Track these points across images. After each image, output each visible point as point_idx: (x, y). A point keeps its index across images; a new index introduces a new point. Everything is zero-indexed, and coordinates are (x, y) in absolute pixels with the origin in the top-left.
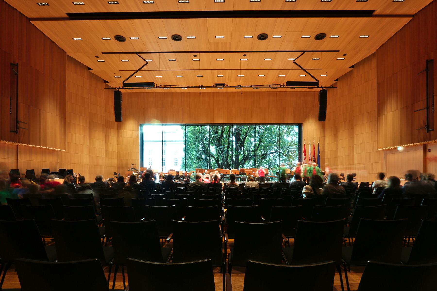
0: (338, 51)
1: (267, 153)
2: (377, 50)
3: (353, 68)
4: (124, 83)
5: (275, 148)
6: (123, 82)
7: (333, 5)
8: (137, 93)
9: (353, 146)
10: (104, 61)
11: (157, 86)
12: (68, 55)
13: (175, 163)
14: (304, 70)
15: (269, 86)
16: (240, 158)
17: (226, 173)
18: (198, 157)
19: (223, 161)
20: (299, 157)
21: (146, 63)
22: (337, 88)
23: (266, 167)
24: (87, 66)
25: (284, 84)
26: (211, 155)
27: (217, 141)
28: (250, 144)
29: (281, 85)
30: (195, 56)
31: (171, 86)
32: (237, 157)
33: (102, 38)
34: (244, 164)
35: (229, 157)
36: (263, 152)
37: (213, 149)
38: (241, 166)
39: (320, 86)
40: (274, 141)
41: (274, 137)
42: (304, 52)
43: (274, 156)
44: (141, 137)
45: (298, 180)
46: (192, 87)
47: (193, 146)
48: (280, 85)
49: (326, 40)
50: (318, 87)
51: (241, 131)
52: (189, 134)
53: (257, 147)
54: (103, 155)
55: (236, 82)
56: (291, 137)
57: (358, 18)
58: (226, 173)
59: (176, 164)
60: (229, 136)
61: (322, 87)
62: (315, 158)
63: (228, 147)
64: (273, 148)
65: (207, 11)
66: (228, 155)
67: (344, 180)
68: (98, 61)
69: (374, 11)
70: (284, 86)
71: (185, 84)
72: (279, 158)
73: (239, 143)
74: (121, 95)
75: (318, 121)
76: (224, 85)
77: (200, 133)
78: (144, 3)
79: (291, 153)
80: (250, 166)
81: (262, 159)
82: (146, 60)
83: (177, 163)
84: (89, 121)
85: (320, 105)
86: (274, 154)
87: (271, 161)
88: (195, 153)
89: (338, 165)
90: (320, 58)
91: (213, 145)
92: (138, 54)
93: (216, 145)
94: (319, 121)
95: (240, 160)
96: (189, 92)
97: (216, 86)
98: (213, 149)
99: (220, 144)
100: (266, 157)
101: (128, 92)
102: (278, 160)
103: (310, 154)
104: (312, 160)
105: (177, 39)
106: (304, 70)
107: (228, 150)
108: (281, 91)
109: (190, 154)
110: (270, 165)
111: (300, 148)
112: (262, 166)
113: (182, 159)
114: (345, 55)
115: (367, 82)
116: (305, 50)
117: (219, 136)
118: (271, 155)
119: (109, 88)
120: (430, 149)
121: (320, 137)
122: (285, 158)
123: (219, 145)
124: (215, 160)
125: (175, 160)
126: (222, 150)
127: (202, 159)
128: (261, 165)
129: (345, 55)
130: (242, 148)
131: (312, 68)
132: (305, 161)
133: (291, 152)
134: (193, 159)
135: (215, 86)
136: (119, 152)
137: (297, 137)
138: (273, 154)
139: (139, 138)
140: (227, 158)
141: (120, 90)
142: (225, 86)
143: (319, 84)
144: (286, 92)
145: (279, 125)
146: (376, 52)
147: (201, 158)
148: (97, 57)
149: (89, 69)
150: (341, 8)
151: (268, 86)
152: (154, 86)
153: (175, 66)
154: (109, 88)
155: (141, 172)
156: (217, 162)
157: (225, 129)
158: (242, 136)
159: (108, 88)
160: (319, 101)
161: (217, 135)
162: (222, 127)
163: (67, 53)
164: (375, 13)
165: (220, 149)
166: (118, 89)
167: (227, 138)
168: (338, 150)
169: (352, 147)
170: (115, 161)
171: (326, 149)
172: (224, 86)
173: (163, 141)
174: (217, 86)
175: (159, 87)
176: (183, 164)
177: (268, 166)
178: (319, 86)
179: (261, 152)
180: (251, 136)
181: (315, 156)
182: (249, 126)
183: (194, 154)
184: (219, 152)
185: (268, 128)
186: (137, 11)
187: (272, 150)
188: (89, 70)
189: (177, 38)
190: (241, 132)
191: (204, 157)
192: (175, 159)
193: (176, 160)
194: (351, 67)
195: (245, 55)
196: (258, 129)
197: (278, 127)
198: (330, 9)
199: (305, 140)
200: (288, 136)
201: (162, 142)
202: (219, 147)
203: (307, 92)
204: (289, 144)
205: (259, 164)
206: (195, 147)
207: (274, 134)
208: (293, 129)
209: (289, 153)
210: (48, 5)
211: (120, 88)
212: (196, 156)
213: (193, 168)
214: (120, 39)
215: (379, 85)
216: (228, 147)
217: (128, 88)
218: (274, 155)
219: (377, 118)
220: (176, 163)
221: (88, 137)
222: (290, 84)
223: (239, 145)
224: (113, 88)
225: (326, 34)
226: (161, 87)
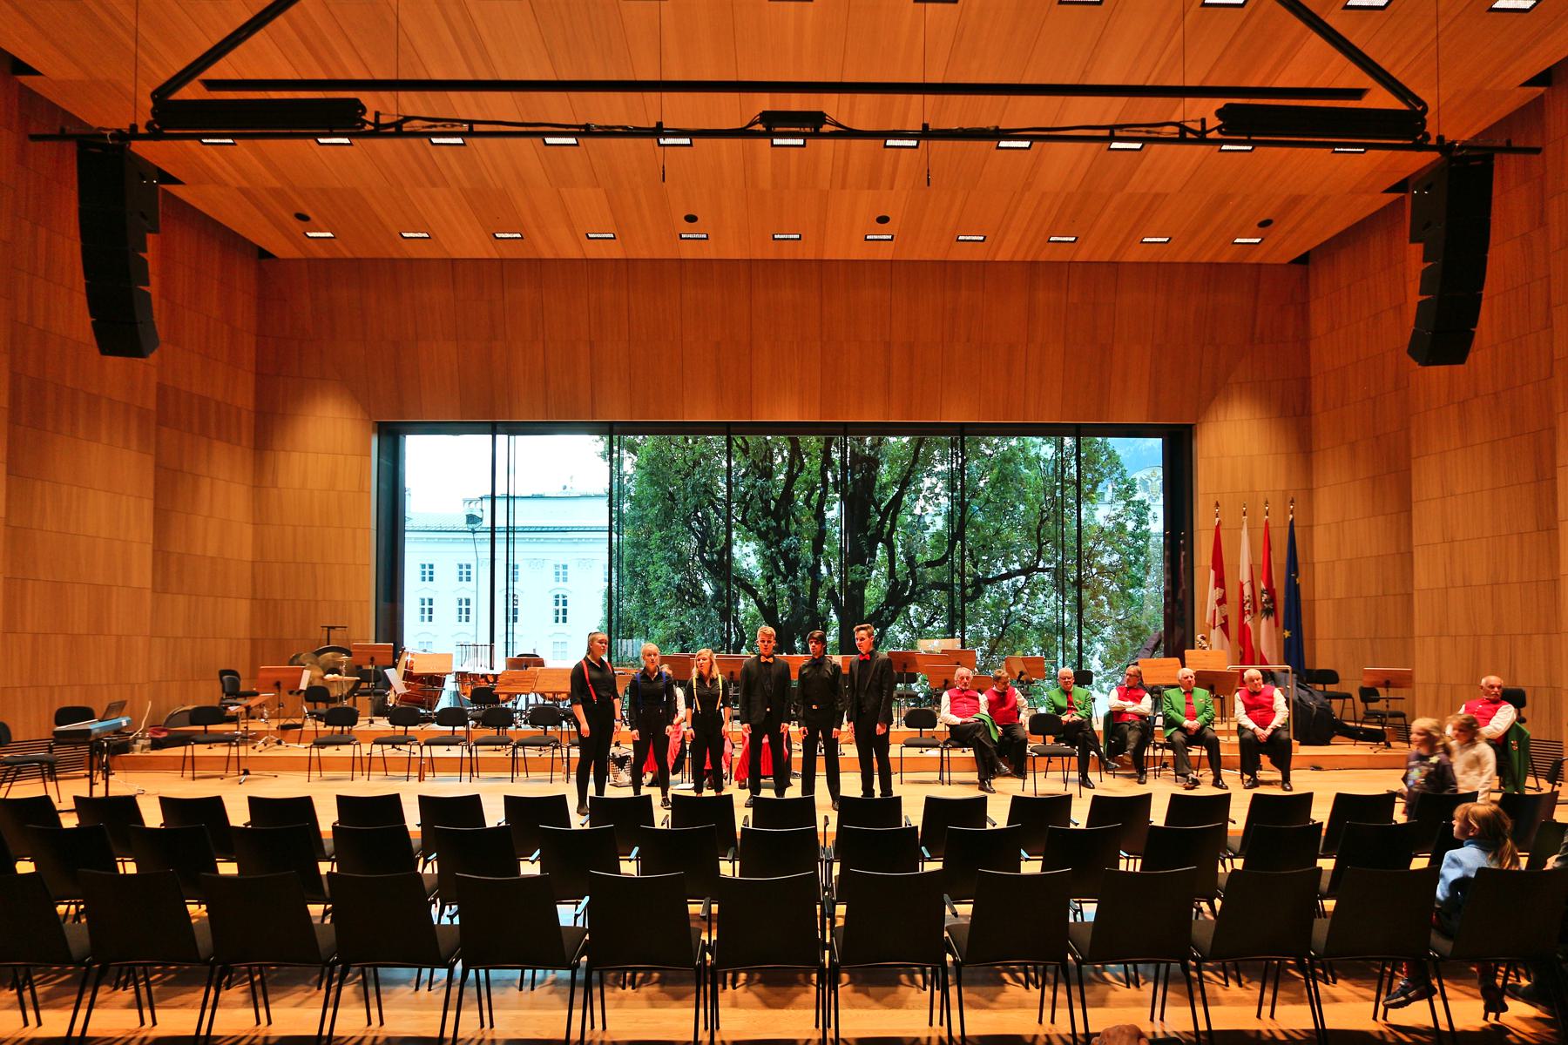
3: (1541, 90)
6: (161, 95)
11: (377, 124)
16: (874, 593)
19: (793, 609)
22: (1538, 151)
25: (1203, 121)
26: (737, 579)
29: (1183, 129)
31: (471, 123)
37: (747, 556)
48: (1176, 129)
50: (1420, 147)
54: (142, 571)
59: (561, 616)
62: (1272, 599)
63: (817, 549)
88: (664, 570)
93: (762, 536)
98: (747, 556)
101: (310, 256)
103: (1245, 576)
104: (1260, 608)
108: (1092, 260)
117: (777, 493)
120: (566, 581)
123: (775, 535)
124: (759, 603)
127: (698, 599)
132: (1221, 611)
135: (760, 127)
140: (814, 596)
142: (826, 128)
151: (1106, 133)
168: (1415, 550)
170: (239, 614)
175: (393, 130)
181: (1275, 586)
188: (19, 77)
194: (1531, 83)
202: (778, 543)
203: (1218, 264)
211: (133, 134)
212: (669, 584)
217: (199, 137)
220: (464, 611)
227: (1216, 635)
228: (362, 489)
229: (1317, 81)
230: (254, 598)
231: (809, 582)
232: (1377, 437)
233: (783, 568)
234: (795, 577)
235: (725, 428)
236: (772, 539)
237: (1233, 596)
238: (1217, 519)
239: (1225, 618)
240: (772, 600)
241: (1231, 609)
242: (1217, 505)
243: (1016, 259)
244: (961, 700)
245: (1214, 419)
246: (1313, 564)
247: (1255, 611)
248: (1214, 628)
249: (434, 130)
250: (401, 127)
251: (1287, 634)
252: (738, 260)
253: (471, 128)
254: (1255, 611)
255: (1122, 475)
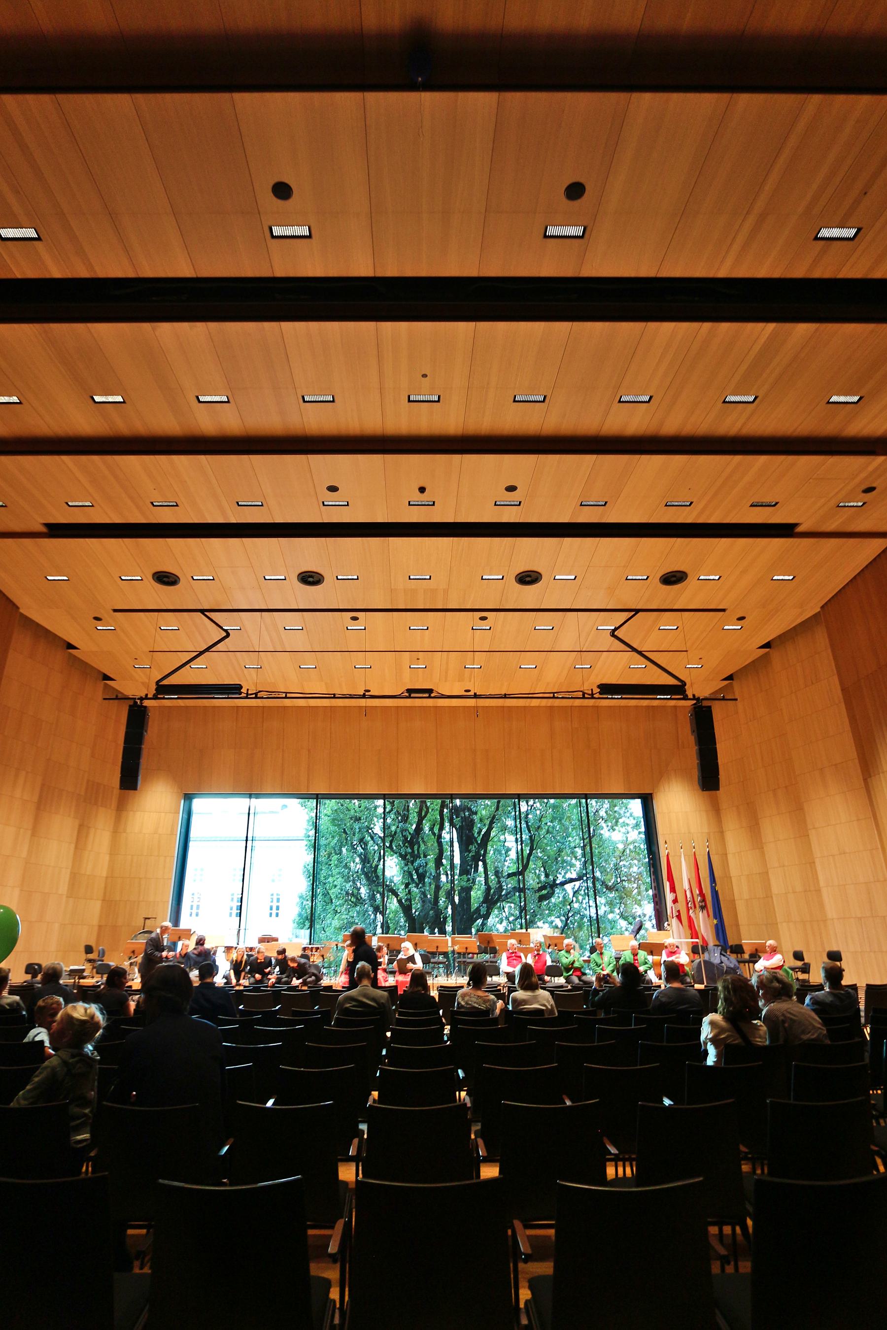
0: (724, 610)
1: (554, 880)
2: (822, 607)
3: (768, 650)
4: (160, 684)
5: (578, 865)
6: (157, 683)
7: (695, 514)
8: (187, 706)
9: (814, 862)
10: (113, 628)
11: (247, 694)
12: (22, 615)
13: (271, 908)
14: (640, 653)
15: (554, 695)
16: (477, 895)
17: (437, 947)
18: (347, 893)
19: (423, 906)
20: (655, 896)
21: (224, 634)
23: (554, 924)
24: (65, 641)
25: (592, 690)
27: (406, 844)
28: (503, 852)
29: (584, 694)
30: (355, 619)
31: (286, 693)
32: (466, 892)
33: (120, 577)
34: (486, 917)
35: (442, 893)
36: (543, 878)
38: (479, 921)
39: (690, 696)
40: (572, 845)
41: (570, 830)
42: (637, 611)
43: (576, 891)
44: (183, 830)
45: (676, 985)
46: (344, 697)
47: (335, 858)
49: (690, 584)
50: (686, 698)
51: (476, 813)
52: (324, 822)
53: (524, 863)
54: (63, 888)
55: (460, 683)
56: (623, 830)
57: (759, 540)
58: (437, 947)
59: (274, 912)
60: (442, 828)
61: (696, 697)
62: (704, 899)
63: (438, 863)
64: (572, 865)
65: (389, 521)
66: (438, 888)
67: (809, 973)
68: (99, 628)
69: (795, 525)
70: (594, 696)
71: (321, 689)
72: (595, 896)
73: (470, 851)
74: (148, 715)
75: (697, 787)
76: (430, 691)
77: (358, 819)
78: (239, 505)
79: (629, 881)
80: (505, 923)
81: (542, 898)
82: (224, 628)
83: (278, 908)
84: (43, 785)
85: (699, 745)
86: (577, 884)
87: (570, 905)
88: (339, 881)
89: (778, 921)
90: (680, 624)
91: (392, 856)
92: (206, 613)
93: (403, 857)
94: (703, 790)
95: (474, 905)
96: (331, 707)
97: (410, 695)
99: (416, 852)
100: (552, 894)
101: (161, 705)
102: (592, 903)
103: (686, 886)
104: (697, 906)
105: (310, 582)
106: (640, 653)
107: (440, 872)
108: (583, 705)
109: (325, 884)
110: (567, 920)
111: (653, 867)
112: (542, 921)
113: (298, 900)
114: (741, 618)
115: (812, 683)
116: (637, 608)
118: (569, 887)
119: (117, 698)
121: (709, 833)
122: (612, 895)
123: (411, 857)
124: (400, 901)
125: (272, 899)
126: (421, 871)
127: (359, 901)
128: (540, 920)
129: (741, 618)
130: (480, 863)
131: (660, 650)
132: (675, 907)
133: (629, 877)
134: (333, 901)
135: (407, 694)
136: (110, 877)
137: (640, 833)
138: (573, 883)
139: (176, 835)
141: (146, 703)
142: (432, 695)
143: (686, 691)
144: (597, 707)
145: (586, 797)
146: (819, 612)
147: (357, 898)
148: (97, 619)
149: (70, 646)
150: (714, 518)
151: (552, 695)
152: (240, 694)
153: (298, 641)
154: (117, 696)
155: (169, 945)
156: (406, 909)
157: (428, 808)
158: (480, 829)
159: (114, 697)
160: (692, 734)
161: (407, 825)
162: (421, 802)
163: (21, 611)
164: (800, 529)
165: (417, 871)
166: (141, 699)
167: (434, 834)
168: (770, 872)
169: (809, 864)
171: (734, 871)
172: (430, 695)
173: (247, 840)
174: (412, 695)
175: (254, 696)
176: (300, 915)
177: (561, 921)
178: (687, 696)
179: (539, 877)
180: (504, 829)
181: (704, 892)
182: (499, 802)
183: (336, 883)
184: (411, 875)
185: (554, 807)
186: (221, 520)
187: (569, 872)
189: (311, 579)
190: (476, 818)
191: (364, 892)
192: (272, 895)
193: (275, 898)
195: (483, 619)
196: (524, 807)
197: (583, 807)
198: (689, 520)
199: (666, 842)
200: (614, 830)
201: (245, 842)
202: (412, 863)
204: (617, 853)
205: (534, 915)
206: (341, 863)
207: (571, 823)
208: (627, 808)
209: (622, 881)
210: (6, 506)
211: (146, 698)
212: (342, 890)
213: (332, 929)
214: (166, 579)
215: (850, 695)
216: (438, 863)
218: (576, 888)
219: (865, 780)
220: (274, 908)
221: (29, 832)
222: (607, 689)
223: (472, 856)
224: (127, 698)
225: (688, 573)
226: (259, 695)
227: (674, 922)
228: (173, 833)
229: (663, 646)
230: (103, 900)
231: (433, 886)
232: (748, 804)
233: (415, 877)
234: (424, 884)
235: (383, 796)
236: (408, 859)
237: (681, 898)
238: (667, 851)
239: (679, 911)
240: (410, 900)
241: (681, 906)
242: (666, 842)
243: (541, 705)
244: (512, 958)
245: (663, 791)
246: (731, 877)
247: (695, 907)
248: (673, 918)
249: (270, 696)
250: (257, 695)
251: (715, 922)
252: (391, 707)
253: (286, 695)
254: (695, 907)
255: (631, 815)
